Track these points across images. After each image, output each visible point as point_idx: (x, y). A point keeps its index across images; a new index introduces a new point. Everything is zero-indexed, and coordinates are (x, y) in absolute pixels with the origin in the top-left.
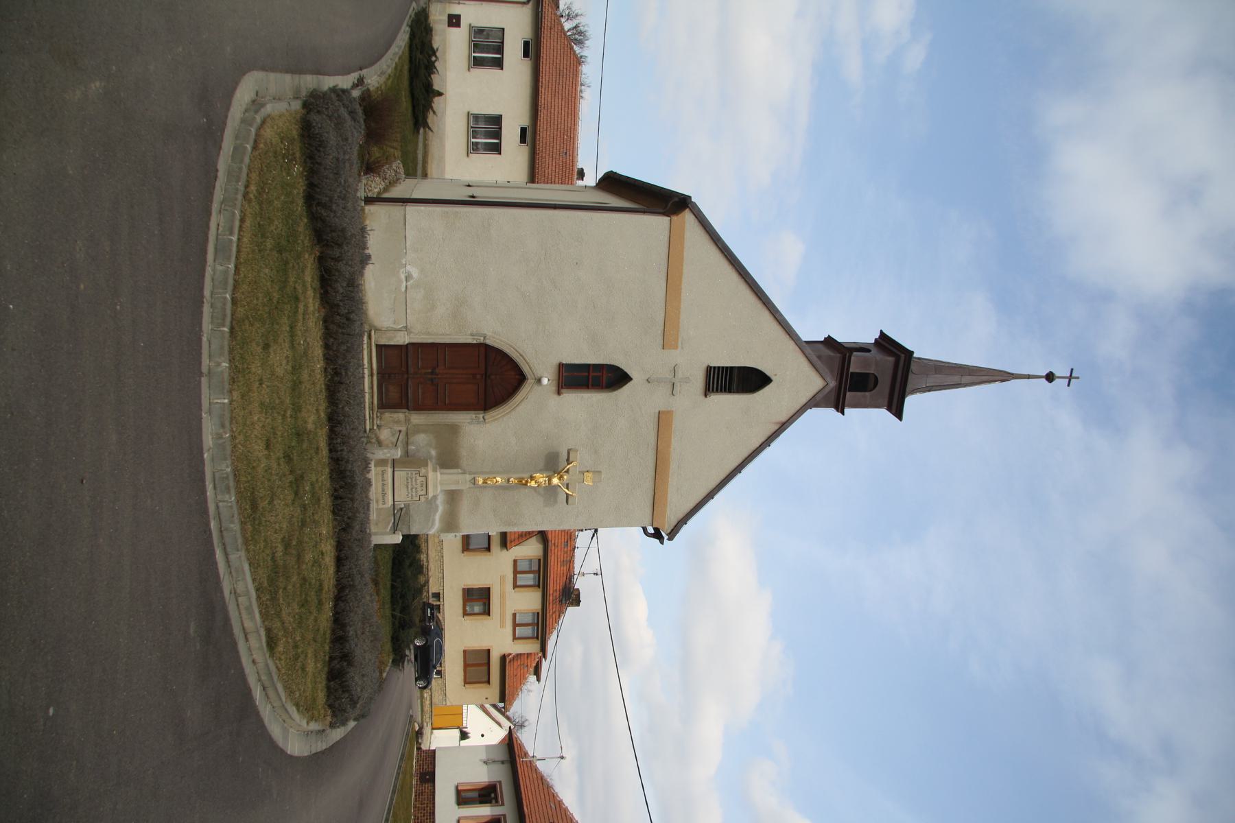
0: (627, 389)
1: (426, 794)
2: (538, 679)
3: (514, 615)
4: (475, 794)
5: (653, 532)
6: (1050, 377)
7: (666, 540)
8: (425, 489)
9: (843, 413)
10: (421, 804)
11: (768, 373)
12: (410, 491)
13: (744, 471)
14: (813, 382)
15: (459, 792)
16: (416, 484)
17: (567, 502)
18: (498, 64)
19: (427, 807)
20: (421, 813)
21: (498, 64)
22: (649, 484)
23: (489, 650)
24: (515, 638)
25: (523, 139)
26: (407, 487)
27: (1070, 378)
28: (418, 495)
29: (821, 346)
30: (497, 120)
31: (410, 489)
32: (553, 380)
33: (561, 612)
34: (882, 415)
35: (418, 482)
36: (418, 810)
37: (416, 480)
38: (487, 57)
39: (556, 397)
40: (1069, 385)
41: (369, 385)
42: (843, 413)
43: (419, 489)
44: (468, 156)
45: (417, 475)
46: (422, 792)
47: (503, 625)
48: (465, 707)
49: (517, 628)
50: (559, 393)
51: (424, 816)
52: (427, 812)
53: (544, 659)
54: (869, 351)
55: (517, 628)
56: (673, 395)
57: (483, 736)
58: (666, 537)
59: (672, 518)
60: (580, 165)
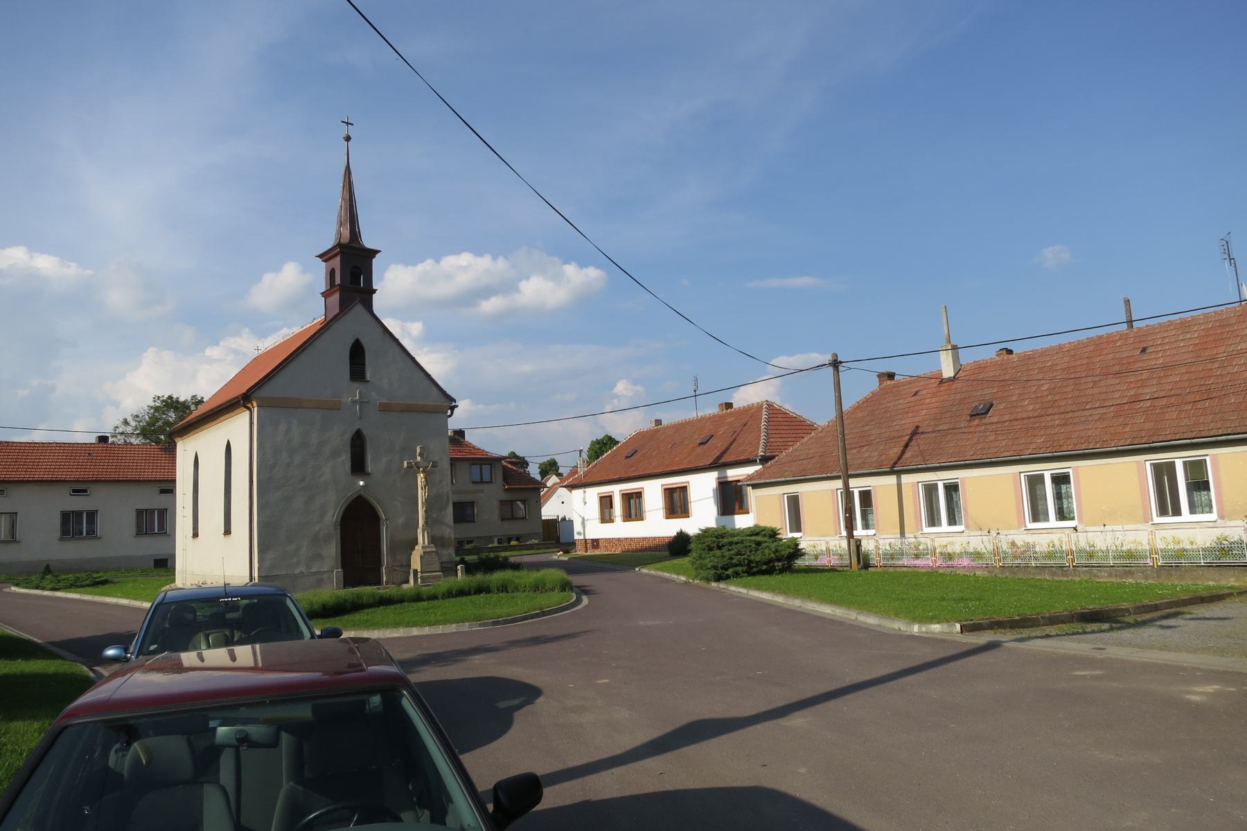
0: (365, 432)
4: (607, 511)
5: (449, 411)
6: (348, 139)
9: (376, 290)
15: (869, 492)
21: (92, 515)
23: (501, 501)
24: (491, 482)
27: (348, 123)
30: (65, 516)
33: (469, 446)
38: (154, 527)
40: (352, 124)
41: (366, 590)
42: (376, 290)
47: (482, 491)
48: (543, 518)
58: (454, 404)
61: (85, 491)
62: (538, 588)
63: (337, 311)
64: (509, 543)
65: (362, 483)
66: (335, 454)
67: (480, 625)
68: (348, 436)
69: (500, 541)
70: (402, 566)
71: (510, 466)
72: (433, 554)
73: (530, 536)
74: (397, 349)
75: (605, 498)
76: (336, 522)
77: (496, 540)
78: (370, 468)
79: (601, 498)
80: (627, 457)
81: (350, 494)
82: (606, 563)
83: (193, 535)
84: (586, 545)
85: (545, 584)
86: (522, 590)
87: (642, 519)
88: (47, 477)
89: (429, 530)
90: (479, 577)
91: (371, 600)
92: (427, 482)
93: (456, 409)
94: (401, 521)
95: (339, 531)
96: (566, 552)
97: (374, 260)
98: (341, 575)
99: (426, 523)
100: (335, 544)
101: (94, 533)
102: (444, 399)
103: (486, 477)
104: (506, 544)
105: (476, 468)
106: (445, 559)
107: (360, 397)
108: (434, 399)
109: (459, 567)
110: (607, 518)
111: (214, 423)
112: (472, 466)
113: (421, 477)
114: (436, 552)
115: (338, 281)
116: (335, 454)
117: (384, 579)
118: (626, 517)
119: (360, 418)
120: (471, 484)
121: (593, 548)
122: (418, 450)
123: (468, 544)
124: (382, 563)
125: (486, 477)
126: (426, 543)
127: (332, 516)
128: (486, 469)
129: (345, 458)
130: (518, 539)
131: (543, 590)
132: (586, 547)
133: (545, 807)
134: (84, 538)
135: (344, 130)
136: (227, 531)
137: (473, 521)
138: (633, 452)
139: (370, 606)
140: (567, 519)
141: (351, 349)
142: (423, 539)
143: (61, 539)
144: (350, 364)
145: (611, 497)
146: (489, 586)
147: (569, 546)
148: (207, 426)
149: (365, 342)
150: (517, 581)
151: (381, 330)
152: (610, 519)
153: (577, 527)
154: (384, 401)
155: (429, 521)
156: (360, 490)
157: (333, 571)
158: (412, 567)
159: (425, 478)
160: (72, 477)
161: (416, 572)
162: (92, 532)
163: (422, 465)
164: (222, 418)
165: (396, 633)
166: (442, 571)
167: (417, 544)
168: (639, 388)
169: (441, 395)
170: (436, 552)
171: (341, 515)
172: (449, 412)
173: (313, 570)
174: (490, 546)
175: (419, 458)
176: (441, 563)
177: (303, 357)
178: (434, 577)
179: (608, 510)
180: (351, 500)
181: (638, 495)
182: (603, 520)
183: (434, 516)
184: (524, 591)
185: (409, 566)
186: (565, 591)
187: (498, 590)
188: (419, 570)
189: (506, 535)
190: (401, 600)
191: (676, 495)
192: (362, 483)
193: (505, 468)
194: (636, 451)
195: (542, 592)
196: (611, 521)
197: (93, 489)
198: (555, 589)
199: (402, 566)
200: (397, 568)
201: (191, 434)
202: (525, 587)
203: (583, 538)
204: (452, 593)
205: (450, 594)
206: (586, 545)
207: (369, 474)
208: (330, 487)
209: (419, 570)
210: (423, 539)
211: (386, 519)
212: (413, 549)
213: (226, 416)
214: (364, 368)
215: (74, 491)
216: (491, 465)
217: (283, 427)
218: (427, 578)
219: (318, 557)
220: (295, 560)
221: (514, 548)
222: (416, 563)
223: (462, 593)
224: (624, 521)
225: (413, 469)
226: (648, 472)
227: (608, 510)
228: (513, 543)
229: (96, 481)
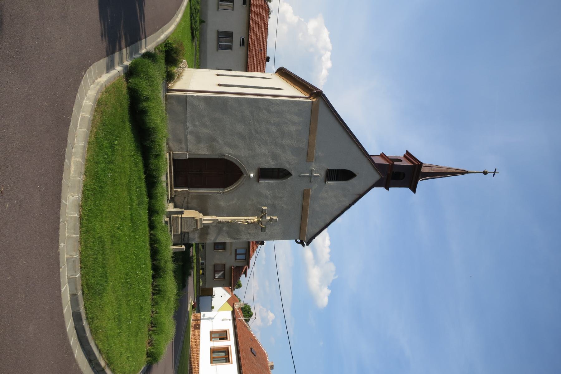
1: (196, 335)
2: (246, 276)
3: (236, 250)
4: (217, 335)
5: (300, 241)
6: (485, 173)
7: (305, 246)
9: (388, 190)
10: (194, 340)
11: (355, 172)
12: (189, 227)
13: (342, 216)
14: (376, 176)
16: (192, 224)
18: (230, 48)
19: (197, 341)
20: (194, 344)
21: (230, 48)
23: (225, 265)
24: (236, 259)
26: (188, 225)
27: (494, 173)
29: (379, 157)
31: (189, 226)
32: (256, 176)
34: (407, 190)
35: (193, 223)
36: (193, 343)
37: (192, 222)
40: (494, 176)
42: (388, 190)
46: (195, 334)
47: (231, 254)
48: (214, 288)
49: (237, 255)
51: (195, 346)
52: (197, 344)
53: (248, 269)
54: (401, 161)
55: (237, 255)
56: (311, 182)
57: (221, 296)
58: (305, 244)
59: (308, 236)
60: (268, 55)
61: (243, 45)
62: (154, 327)
63: (376, 162)
64: (202, 269)
65: (252, 175)
66: (275, 157)
67: (74, 296)
68: (287, 167)
69: (202, 264)
70: (188, 203)
71: (244, 270)
72: (195, 227)
73: (204, 282)
74: (347, 204)
75: (225, 334)
76: (224, 156)
77: (203, 262)
78: (263, 182)
79: (226, 331)
80: (251, 349)
81: (244, 167)
82: (183, 344)
83: (220, 84)
84: (197, 320)
85: (158, 334)
86: (154, 309)
87: (211, 363)
88: (251, 26)
89: (214, 224)
90: (170, 266)
91: (153, 167)
92: (251, 223)
93: (301, 245)
94: (222, 203)
95: (217, 157)
96: (193, 307)
97: (408, 189)
98: (183, 157)
99: (220, 222)
100: (207, 154)
101: (220, 48)
102: (309, 237)
103: (238, 257)
104: (200, 267)
105: (243, 251)
106: (191, 236)
107: (315, 176)
108: (310, 229)
109: (183, 247)
110: (213, 336)
111: (292, 85)
112: (245, 249)
113: (255, 219)
114: (196, 229)
115: (396, 163)
116: (275, 157)
117: (179, 190)
118: (213, 350)
119: (299, 176)
120: (235, 249)
121: (194, 325)
122: (274, 218)
123: (202, 246)
124: (190, 189)
125: (238, 257)
126: (204, 222)
127: (229, 153)
128: (243, 257)
129: (271, 164)
130: (203, 274)
131: (151, 332)
132: (195, 320)
133: (386, 162)
134: (218, 44)
135: (490, 170)
136: (220, 85)
137: (215, 249)
138: (254, 353)
139: (146, 165)
140: (212, 299)
141: (350, 171)
142: (208, 219)
143: (218, 31)
144: (338, 170)
145: (227, 338)
146: (161, 277)
147: (197, 308)
148: (290, 83)
149: (353, 181)
150: (163, 305)
151: (361, 192)
152: (212, 338)
153: (208, 314)
154: (311, 194)
155: (220, 225)
156: (247, 174)
157: (187, 151)
158: (185, 210)
159: (254, 222)
160: (250, 38)
161: (182, 213)
162: (220, 47)
163: (263, 220)
164: (297, 87)
165: (75, 171)
166: (181, 233)
167: (204, 215)
168: (271, 323)
169: (312, 235)
170: (196, 229)
171: (229, 159)
172: (299, 241)
173: (189, 136)
174: (200, 258)
175: (268, 218)
176: (188, 233)
177: (344, 134)
178: (177, 227)
179: (218, 336)
180: (240, 166)
181: (227, 360)
182: (212, 333)
183: (224, 228)
184: (153, 312)
185: (188, 208)
186: (148, 357)
187: (156, 286)
188: (183, 216)
189: (205, 267)
190: (151, 195)
191: (223, 354)
192: (252, 175)
193: (243, 267)
194: (255, 356)
195: (149, 330)
196: (211, 339)
197: (244, 48)
198: (150, 346)
199: (188, 203)
200: (186, 200)
201: (283, 78)
202: (157, 313)
203: (201, 318)
204: (155, 244)
205: (154, 242)
206: (197, 320)
207: (258, 181)
208: (250, 152)
209: (183, 216)
210: (208, 219)
211: (224, 193)
212: (200, 212)
213: (300, 89)
214: (334, 180)
215: (243, 39)
216: (246, 259)
217: (296, 119)
218: (176, 222)
219: (199, 140)
220: (197, 123)
221: (198, 272)
222: (188, 214)
223: (155, 253)
224: (211, 348)
225: (261, 213)
226: (243, 368)
227: (218, 336)
228: (201, 271)
229: (248, 50)
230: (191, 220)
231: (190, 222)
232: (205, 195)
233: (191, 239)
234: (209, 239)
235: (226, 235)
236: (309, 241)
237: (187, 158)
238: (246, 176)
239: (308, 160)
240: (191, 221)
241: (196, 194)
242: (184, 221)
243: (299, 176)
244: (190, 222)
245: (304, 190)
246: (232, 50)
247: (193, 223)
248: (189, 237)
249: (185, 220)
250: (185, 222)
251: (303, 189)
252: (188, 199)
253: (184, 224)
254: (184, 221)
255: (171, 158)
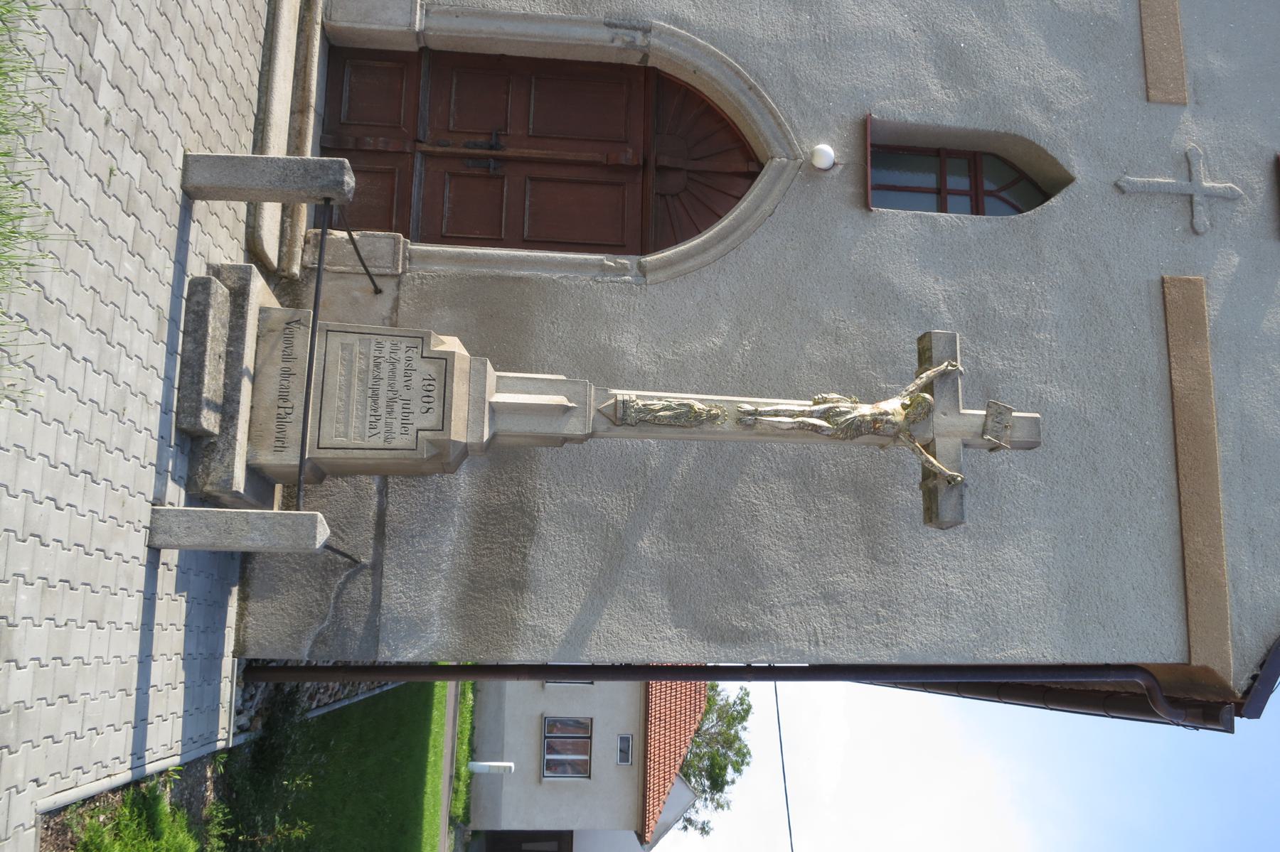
8: (436, 406)
12: (382, 411)
17: (931, 514)
18: (584, 770)
21: (584, 770)
22: (1160, 515)
25: (624, 754)
26: (375, 397)
28: (412, 430)
31: (382, 402)
35: (416, 380)
39: (857, 213)
43: (416, 406)
44: (540, 781)
45: (415, 354)
50: (867, 206)
56: (1196, 233)
72: (431, 420)
76: (647, 31)
107: (1210, 195)
119: (1118, 188)
154: (1212, 309)
230: (401, 355)
231: (393, 371)
232: (520, 279)
233: (397, 621)
234: (533, 628)
235: (657, 601)
236: (1254, 678)
237: (412, 24)
238: (783, 168)
239: (1152, 92)
240: (401, 367)
241: (454, 270)
242: (349, 364)
243: (1118, 188)
244: (393, 371)
245: (1163, 281)
246: (589, 777)
247: (416, 380)
248: (385, 602)
249: (357, 349)
250: (358, 365)
251: (1156, 278)
252: (397, 299)
253: (349, 385)
254: (349, 364)
255: (313, 21)
